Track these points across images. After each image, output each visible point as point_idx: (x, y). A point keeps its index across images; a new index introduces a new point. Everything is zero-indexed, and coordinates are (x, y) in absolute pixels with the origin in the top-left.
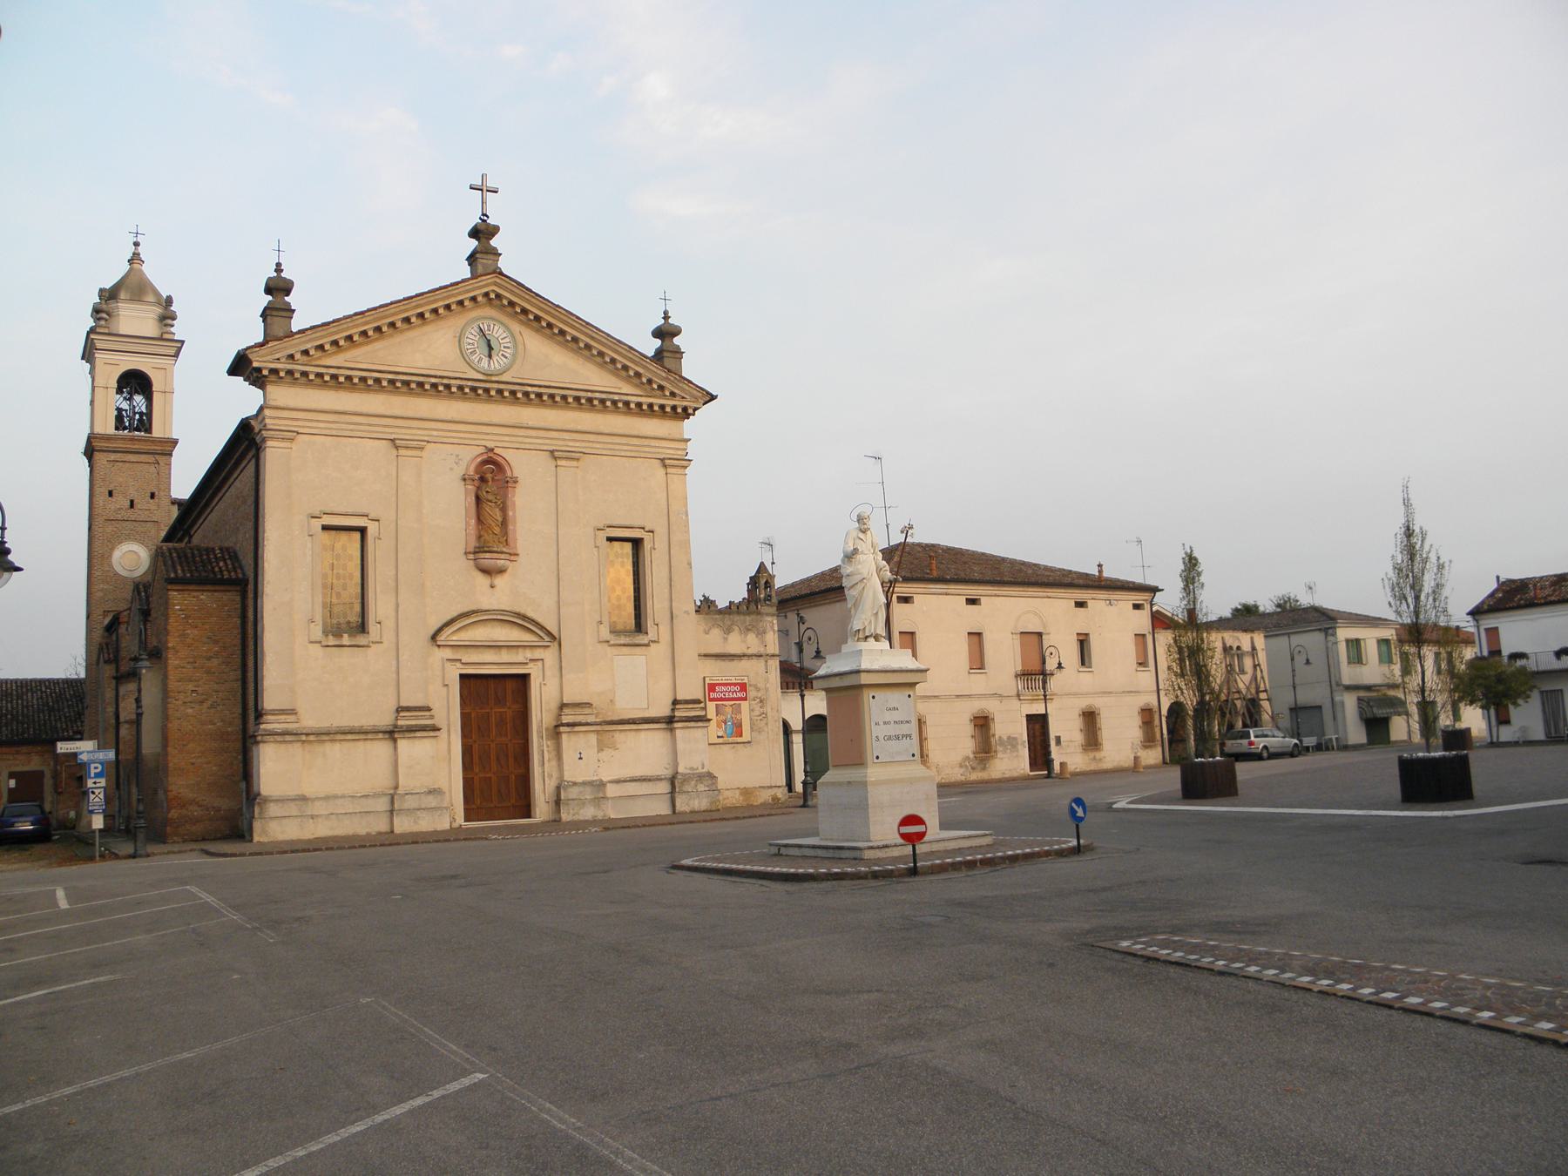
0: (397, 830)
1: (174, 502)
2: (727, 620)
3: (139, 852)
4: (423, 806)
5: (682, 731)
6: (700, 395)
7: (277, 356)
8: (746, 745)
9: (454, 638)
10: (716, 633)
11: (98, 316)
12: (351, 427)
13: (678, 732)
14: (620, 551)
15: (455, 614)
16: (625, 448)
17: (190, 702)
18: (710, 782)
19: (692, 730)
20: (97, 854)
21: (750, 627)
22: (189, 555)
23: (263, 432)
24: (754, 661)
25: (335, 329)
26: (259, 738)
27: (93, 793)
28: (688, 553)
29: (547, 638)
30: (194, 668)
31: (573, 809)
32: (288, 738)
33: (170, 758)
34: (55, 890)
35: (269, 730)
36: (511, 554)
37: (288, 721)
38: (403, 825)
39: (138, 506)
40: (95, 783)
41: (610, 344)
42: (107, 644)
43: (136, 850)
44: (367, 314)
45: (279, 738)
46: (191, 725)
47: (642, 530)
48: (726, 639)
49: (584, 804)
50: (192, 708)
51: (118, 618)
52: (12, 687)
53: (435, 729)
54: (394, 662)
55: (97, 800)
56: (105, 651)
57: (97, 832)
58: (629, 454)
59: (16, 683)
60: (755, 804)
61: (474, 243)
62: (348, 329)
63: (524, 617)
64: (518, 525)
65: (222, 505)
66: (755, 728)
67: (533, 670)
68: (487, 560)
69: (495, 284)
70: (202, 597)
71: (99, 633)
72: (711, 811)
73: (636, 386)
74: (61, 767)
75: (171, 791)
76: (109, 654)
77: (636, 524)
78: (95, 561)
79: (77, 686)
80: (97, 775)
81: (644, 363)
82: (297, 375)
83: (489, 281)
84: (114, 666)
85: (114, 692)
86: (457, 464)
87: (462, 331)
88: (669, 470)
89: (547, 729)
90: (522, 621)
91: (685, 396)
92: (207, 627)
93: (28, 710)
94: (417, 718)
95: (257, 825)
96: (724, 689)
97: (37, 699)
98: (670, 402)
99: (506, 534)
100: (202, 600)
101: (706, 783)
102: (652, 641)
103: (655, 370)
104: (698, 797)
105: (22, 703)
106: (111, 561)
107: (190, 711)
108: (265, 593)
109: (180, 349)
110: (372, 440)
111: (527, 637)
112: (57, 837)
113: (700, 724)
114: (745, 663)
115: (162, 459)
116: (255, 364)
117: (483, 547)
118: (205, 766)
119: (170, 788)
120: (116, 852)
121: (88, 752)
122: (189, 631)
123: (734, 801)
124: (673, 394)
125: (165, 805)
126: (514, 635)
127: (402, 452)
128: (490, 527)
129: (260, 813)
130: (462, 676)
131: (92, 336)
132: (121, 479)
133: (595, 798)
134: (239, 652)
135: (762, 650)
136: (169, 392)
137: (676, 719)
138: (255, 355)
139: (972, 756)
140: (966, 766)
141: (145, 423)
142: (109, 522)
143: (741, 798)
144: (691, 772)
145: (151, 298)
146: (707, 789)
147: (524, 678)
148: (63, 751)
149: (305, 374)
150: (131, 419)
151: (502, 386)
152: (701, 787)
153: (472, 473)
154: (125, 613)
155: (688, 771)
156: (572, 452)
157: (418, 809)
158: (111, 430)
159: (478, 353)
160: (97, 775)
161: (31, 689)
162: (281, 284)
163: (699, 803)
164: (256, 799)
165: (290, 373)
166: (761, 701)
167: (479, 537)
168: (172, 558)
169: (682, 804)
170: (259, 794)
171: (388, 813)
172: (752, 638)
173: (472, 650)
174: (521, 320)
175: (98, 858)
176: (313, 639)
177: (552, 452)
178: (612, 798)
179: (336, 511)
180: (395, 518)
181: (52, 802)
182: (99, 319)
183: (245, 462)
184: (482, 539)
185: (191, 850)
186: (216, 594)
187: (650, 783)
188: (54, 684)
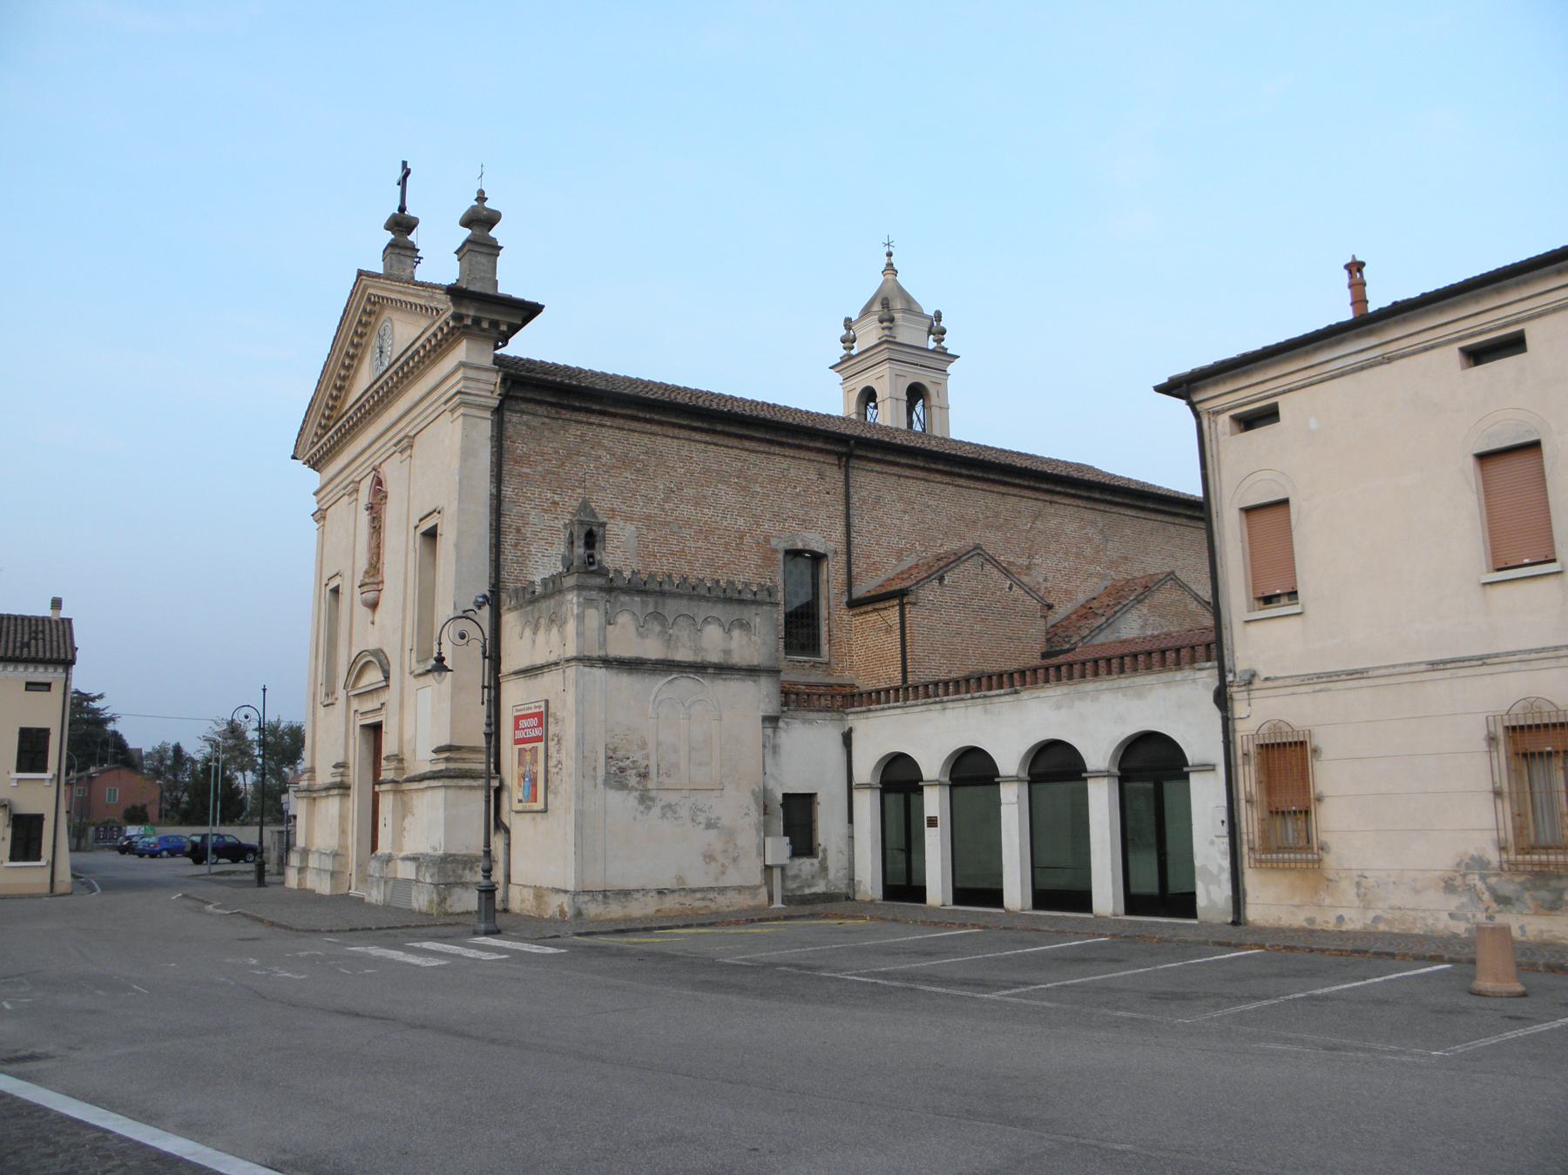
7: (308, 448)
139: (1493, 856)
140: (1471, 889)
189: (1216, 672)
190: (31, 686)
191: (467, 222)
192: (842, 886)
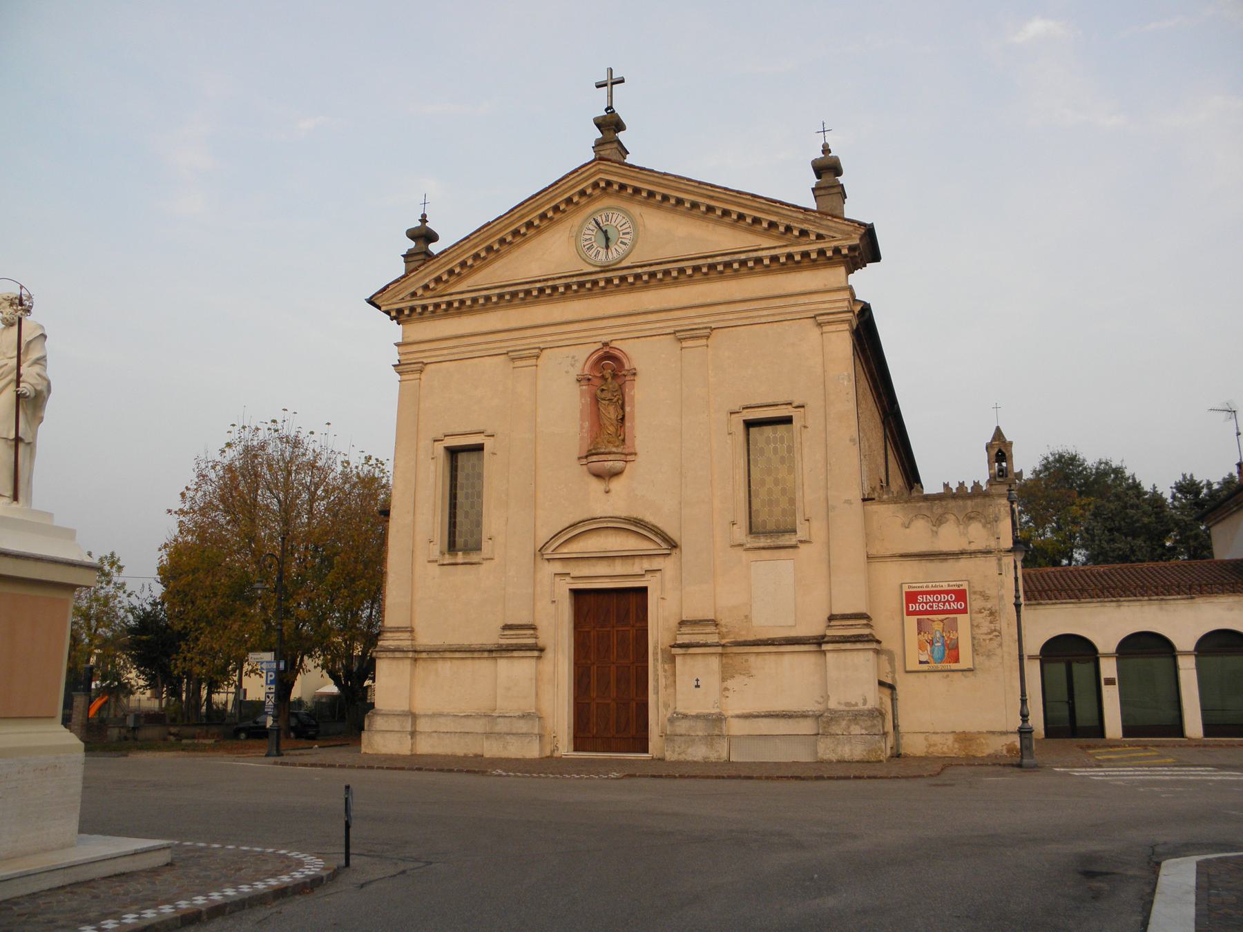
2: (938, 508)
4: (514, 731)
5: (835, 655)
6: (852, 229)
7: (401, 297)
8: (967, 673)
9: (565, 551)
10: (920, 525)
14: (771, 435)
16: (765, 313)
18: (869, 723)
19: (848, 654)
21: (972, 515)
24: (979, 561)
29: (664, 546)
32: (398, 655)
36: (626, 455)
37: (401, 638)
49: (693, 741)
55: (270, 703)
58: (770, 319)
60: (980, 755)
67: (649, 582)
77: (782, 400)
81: (776, 210)
83: (593, 170)
86: (572, 365)
90: (636, 526)
94: (518, 637)
98: (813, 247)
102: (801, 542)
103: (789, 213)
110: (491, 357)
114: (964, 563)
121: (267, 662)
123: (945, 749)
129: (368, 726)
130: (576, 593)
135: (993, 544)
138: (380, 300)
143: (956, 746)
144: (847, 709)
146: (864, 732)
147: (644, 590)
152: (856, 730)
155: (842, 707)
156: (696, 329)
163: (851, 750)
172: (976, 530)
173: (581, 563)
176: (432, 558)
187: (791, 721)
190: (582, 270)
191: (412, 234)
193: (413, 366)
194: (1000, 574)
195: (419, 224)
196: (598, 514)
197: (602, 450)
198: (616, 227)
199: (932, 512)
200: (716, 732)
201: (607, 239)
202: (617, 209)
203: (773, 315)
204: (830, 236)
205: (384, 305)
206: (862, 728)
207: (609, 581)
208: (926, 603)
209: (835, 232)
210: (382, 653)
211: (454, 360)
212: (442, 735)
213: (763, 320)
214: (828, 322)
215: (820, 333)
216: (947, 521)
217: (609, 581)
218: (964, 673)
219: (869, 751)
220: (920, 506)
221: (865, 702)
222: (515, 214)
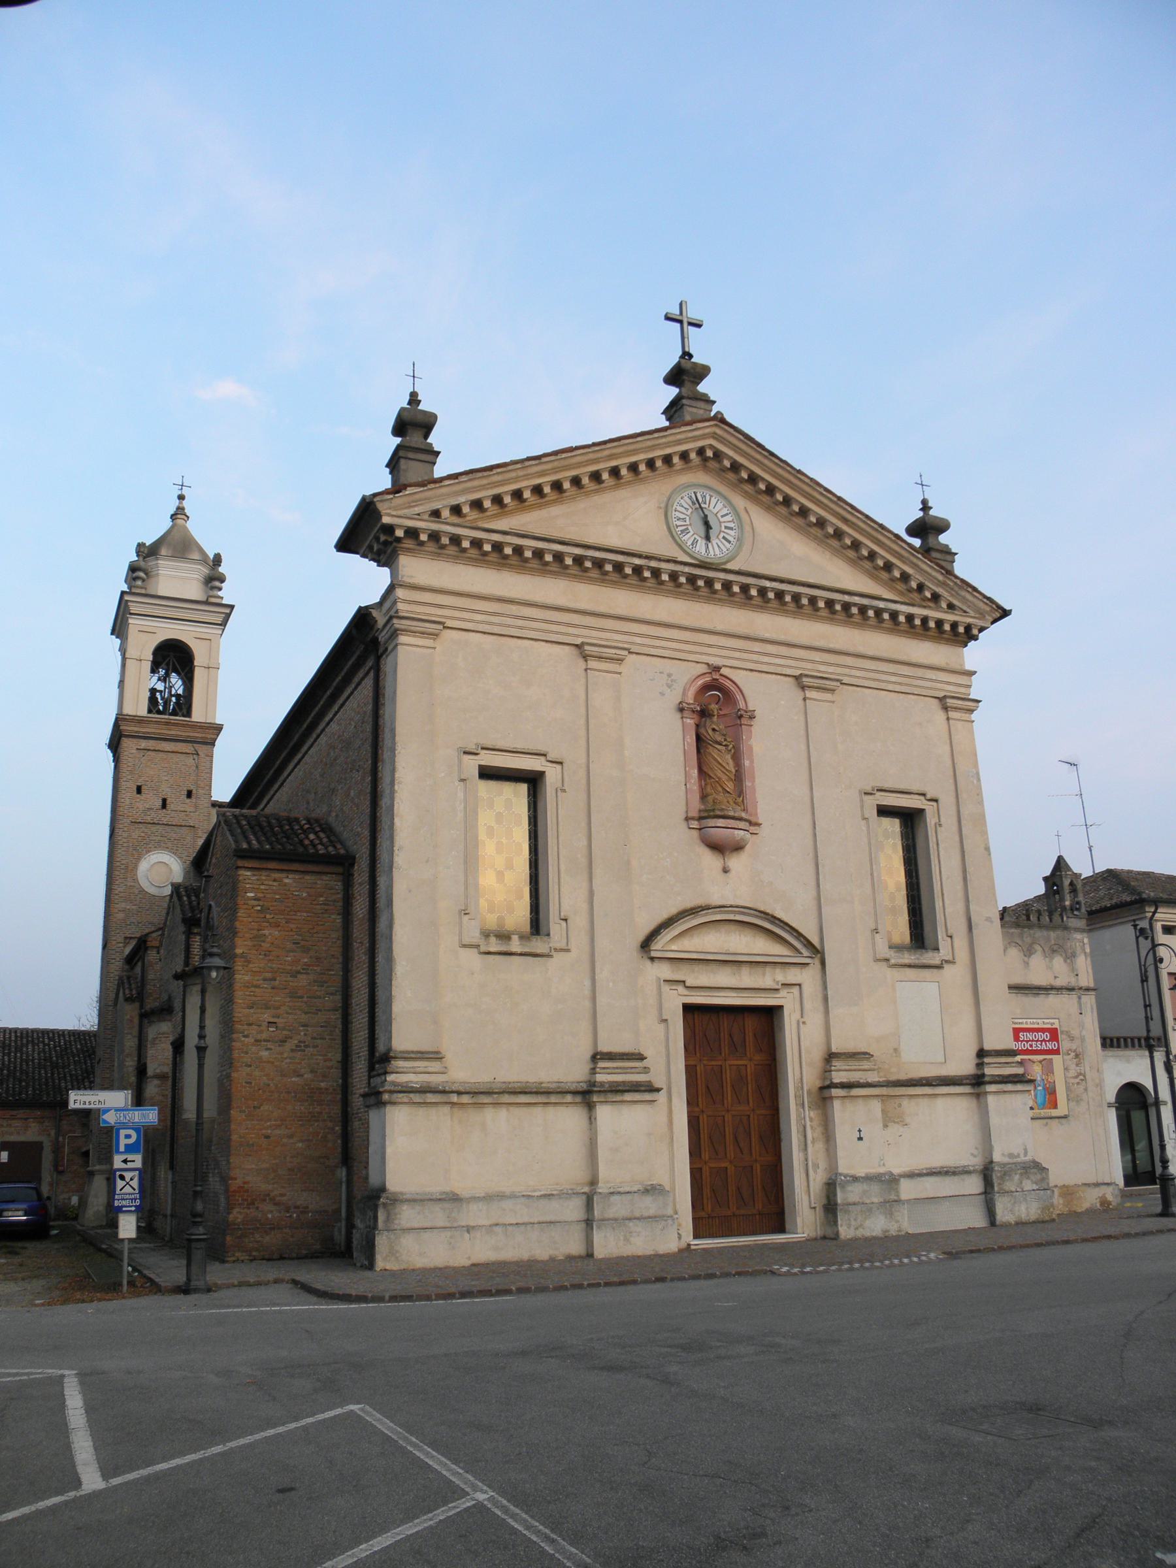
0: (600, 1252)
1: (215, 804)
3: (194, 1283)
4: (638, 1215)
6: (988, 609)
7: (417, 510)
8: (1063, 1121)
9: (674, 947)
11: (134, 575)
12: (520, 623)
13: (991, 1099)
15: (674, 911)
16: (893, 679)
17: (265, 1041)
18: (1039, 1177)
19: (1007, 1096)
20: (125, 1282)
21: (1055, 948)
22: (265, 824)
23: (395, 621)
25: (499, 478)
26: (386, 1097)
27: (122, 1178)
28: (984, 833)
29: (805, 952)
30: (273, 988)
31: (855, 1220)
32: (431, 1098)
33: (233, 1127)
34: (63, 1376)
35: (397, 1084)
37: (430, 1070)
38: (607, 1245)
39: (170, 806)
40: (125, 1161)
41: (869, 529)
42: (129, 978)
43: (189, 1280)
44: (544, 460)
45: (417, 1098)
46: (267, 1075)
47: (922, 798)
48: (1027, 964)
49: (870, 1210)
50: (267, 1049)
51: (145, 942)
52: (10, 1037)
53: (652, 1089)
54: (587, 983)
55: (128, 1189)
56: (127, 986)
57: (126, 1242)
58: (898, 688)
59: (16, 1032)
61: (673, 391)
62: (517, 479)
63: (774, 919)
64: (757, 781)
65: (299, 772)
66: (1072, 1096)
67: (786, 1000)
68: (720, 830)
69: (714, 436)
70: (287, 881)
71: (117, 965)
72: (1043, 1222)
73: (901, 593)
74: (64, 1139)
75: (236, 1179)
76: (131, 990)
78: (117, 873)
79: (85, 1039)
80: (130, 1149)
81: (915, 560)
82: (445, 540)
83: (707, 431)
84: (137, 1005)
85: (136, 1040)
86: (669, 686)
87: (669, 499)
88: (952, 714)
89: (809, 1092)
91: (968, 610)
92: (293, 926)
93: (27, 1065)
94: (625, 1071)
95: (382, 1242)
96: (1030, 1036)
97: (39, 1054)
99: (741, 793)
100: (285, 885)
101: (1032, 1177)
104: (1025, 1200)
105: (21, 1057)
106: (136, 875)
107: (265, 1054)
108: (395, 865)
109: (228, 616)
111: (776, 950)
112: (55, 1232)
113: (1019, 1087)
115: (202, 750)
116: (386, 520)
117: (713, 810)
118: (285, 1140)
119: (232, 1174)
120: (152, 1276)
121: (117, 1110)
122: (266, 932)
124: (951, 606)
125: (222, 1199)
126: (760, 946)
127: (592, 664)
128: (719, 782)
130: (688, 1009)
131: (127, 598)
132: (152, 773)
133: (885, 1202)
134: (339, 967)
135: (1073, 982)
136: (213, 668)
137: (987, 1079)
138: (386, 505)
141: (184, 705)
142: (136, 825)
144: (1011, 1161)
145: (196, 556)
146: (1035, 1187)
147: (771, 1015)
148: (77, 1106)
149: (456, 540)
150: (166, 702)
151: (731, 577)
152: (1028, 1185)
153: (691, 702)
154: (154, 935)
157: (630, 1219)
158: (143, 710)
159: (692, 533)
160: (130, 1149)
161: (33, 1041)
162: (420, 418)
163: (1027, 1209)
164: (379, 1198)
165: (435, 536)
166: (1077, 1056)
167: (704, 797)
168: (241, 827)
169: (1005, 1212)
170: (383, 1189)
171: (583, 1225)
173: (697, 967)
174: (746, 492)
175: (125, 1288)
176: (466, 941)
177: (797, 678)
178: (908, 1201)
179: (499, 745)
180: (583, 760)
181: (51, 1184)
182: (135, 579)
183: (361, 674)
184: (710, 799)
185: (276, 1281)
186: (307, 877)
187: (956, 1178)
188: (59, 1036)
189: (1164, 1053)
192: (384, 1238)
193: (427, 625)
194: (1081, 1014)
195: (921, 514)
196: (716, 900)
197: (731, 813)
198: (716, 515)
199: (1023, 941)
200: (893, 1197)
201: (707, 525)
202: (719, 493)
203: (900, 684)
204: (961, 609)
205: (389, 515)
206: (1033, 1182)
207: (735, 995)
208: (1027, 1041)
209: (969, 607)
210: (401, 1095)
211: (489, 633)
212: (510, 1228)
213: (890, 687)
214: (955, 708)
215: (802, 698)
216: (1036, 951)
217: (735, 995)
218: (1060, 1120)
219: (1043, 1209)
220: (1013, 933)
221: (1026, 1154)
222: (604, 449)
